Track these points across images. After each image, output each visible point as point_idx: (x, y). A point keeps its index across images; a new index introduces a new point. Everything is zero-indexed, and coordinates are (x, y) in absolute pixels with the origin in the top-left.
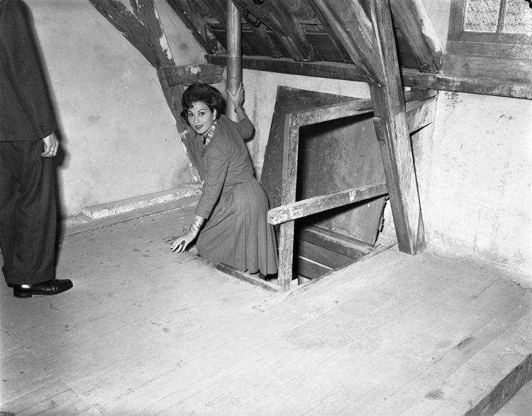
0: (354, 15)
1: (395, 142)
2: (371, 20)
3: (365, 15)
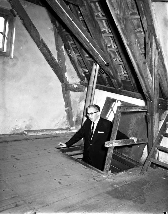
0: (147, 75)
1: (154, 123)
2: (152, 78)
3: (151, 76)
